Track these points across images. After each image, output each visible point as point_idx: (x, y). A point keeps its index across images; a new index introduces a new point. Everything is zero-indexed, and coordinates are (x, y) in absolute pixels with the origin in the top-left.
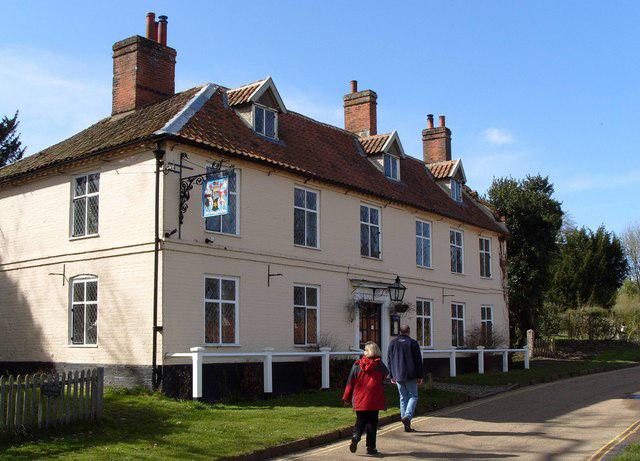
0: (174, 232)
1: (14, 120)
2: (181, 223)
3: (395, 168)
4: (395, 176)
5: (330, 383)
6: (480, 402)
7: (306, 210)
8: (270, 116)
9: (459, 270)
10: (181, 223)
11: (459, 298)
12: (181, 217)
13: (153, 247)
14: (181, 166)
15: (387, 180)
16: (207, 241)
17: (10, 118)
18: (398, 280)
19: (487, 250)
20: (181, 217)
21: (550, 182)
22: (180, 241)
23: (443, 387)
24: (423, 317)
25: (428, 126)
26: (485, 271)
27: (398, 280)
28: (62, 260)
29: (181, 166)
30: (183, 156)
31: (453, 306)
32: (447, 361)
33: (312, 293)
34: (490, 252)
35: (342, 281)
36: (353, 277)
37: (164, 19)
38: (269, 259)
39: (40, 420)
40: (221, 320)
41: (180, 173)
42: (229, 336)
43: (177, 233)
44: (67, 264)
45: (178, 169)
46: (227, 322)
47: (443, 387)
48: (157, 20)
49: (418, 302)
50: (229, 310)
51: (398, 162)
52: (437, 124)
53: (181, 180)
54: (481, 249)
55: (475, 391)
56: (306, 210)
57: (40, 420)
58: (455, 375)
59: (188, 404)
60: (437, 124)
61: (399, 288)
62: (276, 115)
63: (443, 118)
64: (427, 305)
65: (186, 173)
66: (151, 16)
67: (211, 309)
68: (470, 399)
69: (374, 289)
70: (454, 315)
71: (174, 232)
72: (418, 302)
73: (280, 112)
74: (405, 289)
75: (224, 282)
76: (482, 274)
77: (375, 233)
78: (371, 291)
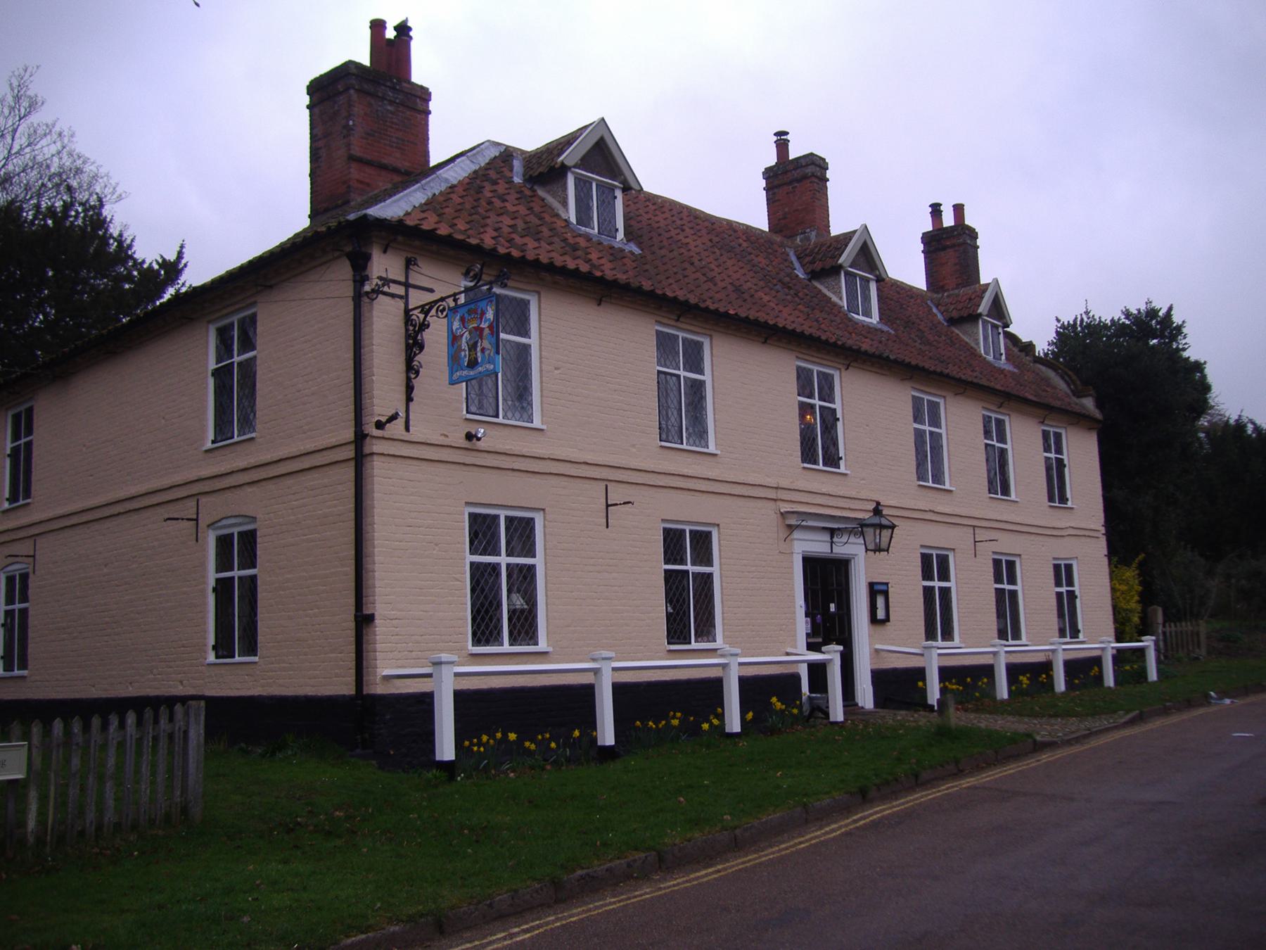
0: (394, 417)
1: (180, 255)
2: (409, 399)
3: (866, 298)
4: (867, 313)
5: (845, 713)
6: (1060, 753)
7: (682, 373)
8: (607, 192)
9: (1006, 490)
10: (409, 399)
11: (1007, 545)
12: (409, 389)
13: (349, 452)
14: (407, 285)
15: (851, 320)
16: (470, 437)
17: (171, 257)
18: (877, 511)
19: (1059, 450)
20: (409, 389)
21: (1177, 319)
22: (407, 436)
23: (984, 722)
24: (937, 584)
25: (928, 227)
26: (1057, 490)
27: (877, 511)
28: (198, 490)
29: (407, 285)
30: (409, 263)
31: (997, 563)
32: (988, 670)
33: (702, 542)
34: (1076, 588)
35: (765, 517)
36: (786, 508)
37: (403, 29)
38: (605, 473)
39: (31, 824)
40: (506, 602)
41: (405, 298)
42: (524, 627)
43: (400, 422)
44: (203, 500)
45: (400, 290)
46: (519, 602)
47: (984, 722)
48: (390, 34)
49: (923, 555)
50: (524, 579)
51: (873, 287)
52: (948, 220)
53: (407, 312)
54: (1046, 451)
55: (1043, 730)
56: (682, 373)
57: (31, 824)
58: (1006, 696)
59: (922, 719)
60: (948, 220)
61: (882, 527)
62: (619, 194)
63: (959, 209)
64: (943, 562)
65: (417, 298)
66: (377, 26)
67: (483, 579)
68: (1039, 747)
69: (832, 532)
70: (998, 579)
71: (394, 417)
72: (923, 555)
73: (626, 189)
74: (893, 527)
75: (510, 520)
76: (1051, 499)
77: (830, 420)
78: (827, 537)
